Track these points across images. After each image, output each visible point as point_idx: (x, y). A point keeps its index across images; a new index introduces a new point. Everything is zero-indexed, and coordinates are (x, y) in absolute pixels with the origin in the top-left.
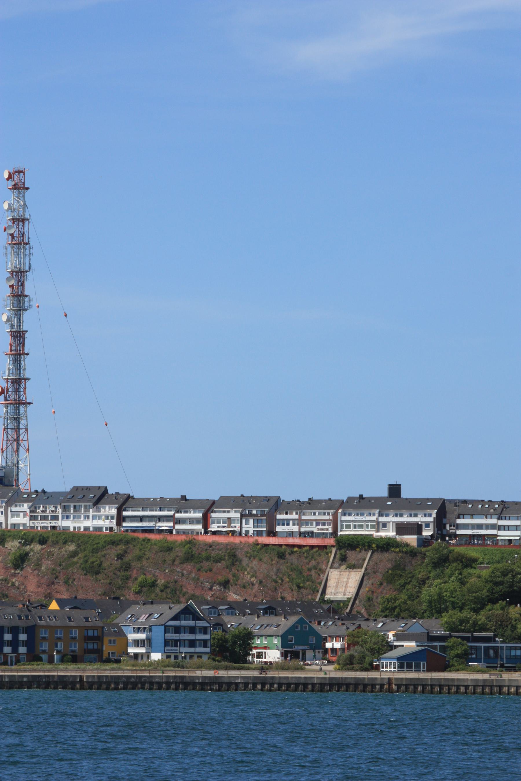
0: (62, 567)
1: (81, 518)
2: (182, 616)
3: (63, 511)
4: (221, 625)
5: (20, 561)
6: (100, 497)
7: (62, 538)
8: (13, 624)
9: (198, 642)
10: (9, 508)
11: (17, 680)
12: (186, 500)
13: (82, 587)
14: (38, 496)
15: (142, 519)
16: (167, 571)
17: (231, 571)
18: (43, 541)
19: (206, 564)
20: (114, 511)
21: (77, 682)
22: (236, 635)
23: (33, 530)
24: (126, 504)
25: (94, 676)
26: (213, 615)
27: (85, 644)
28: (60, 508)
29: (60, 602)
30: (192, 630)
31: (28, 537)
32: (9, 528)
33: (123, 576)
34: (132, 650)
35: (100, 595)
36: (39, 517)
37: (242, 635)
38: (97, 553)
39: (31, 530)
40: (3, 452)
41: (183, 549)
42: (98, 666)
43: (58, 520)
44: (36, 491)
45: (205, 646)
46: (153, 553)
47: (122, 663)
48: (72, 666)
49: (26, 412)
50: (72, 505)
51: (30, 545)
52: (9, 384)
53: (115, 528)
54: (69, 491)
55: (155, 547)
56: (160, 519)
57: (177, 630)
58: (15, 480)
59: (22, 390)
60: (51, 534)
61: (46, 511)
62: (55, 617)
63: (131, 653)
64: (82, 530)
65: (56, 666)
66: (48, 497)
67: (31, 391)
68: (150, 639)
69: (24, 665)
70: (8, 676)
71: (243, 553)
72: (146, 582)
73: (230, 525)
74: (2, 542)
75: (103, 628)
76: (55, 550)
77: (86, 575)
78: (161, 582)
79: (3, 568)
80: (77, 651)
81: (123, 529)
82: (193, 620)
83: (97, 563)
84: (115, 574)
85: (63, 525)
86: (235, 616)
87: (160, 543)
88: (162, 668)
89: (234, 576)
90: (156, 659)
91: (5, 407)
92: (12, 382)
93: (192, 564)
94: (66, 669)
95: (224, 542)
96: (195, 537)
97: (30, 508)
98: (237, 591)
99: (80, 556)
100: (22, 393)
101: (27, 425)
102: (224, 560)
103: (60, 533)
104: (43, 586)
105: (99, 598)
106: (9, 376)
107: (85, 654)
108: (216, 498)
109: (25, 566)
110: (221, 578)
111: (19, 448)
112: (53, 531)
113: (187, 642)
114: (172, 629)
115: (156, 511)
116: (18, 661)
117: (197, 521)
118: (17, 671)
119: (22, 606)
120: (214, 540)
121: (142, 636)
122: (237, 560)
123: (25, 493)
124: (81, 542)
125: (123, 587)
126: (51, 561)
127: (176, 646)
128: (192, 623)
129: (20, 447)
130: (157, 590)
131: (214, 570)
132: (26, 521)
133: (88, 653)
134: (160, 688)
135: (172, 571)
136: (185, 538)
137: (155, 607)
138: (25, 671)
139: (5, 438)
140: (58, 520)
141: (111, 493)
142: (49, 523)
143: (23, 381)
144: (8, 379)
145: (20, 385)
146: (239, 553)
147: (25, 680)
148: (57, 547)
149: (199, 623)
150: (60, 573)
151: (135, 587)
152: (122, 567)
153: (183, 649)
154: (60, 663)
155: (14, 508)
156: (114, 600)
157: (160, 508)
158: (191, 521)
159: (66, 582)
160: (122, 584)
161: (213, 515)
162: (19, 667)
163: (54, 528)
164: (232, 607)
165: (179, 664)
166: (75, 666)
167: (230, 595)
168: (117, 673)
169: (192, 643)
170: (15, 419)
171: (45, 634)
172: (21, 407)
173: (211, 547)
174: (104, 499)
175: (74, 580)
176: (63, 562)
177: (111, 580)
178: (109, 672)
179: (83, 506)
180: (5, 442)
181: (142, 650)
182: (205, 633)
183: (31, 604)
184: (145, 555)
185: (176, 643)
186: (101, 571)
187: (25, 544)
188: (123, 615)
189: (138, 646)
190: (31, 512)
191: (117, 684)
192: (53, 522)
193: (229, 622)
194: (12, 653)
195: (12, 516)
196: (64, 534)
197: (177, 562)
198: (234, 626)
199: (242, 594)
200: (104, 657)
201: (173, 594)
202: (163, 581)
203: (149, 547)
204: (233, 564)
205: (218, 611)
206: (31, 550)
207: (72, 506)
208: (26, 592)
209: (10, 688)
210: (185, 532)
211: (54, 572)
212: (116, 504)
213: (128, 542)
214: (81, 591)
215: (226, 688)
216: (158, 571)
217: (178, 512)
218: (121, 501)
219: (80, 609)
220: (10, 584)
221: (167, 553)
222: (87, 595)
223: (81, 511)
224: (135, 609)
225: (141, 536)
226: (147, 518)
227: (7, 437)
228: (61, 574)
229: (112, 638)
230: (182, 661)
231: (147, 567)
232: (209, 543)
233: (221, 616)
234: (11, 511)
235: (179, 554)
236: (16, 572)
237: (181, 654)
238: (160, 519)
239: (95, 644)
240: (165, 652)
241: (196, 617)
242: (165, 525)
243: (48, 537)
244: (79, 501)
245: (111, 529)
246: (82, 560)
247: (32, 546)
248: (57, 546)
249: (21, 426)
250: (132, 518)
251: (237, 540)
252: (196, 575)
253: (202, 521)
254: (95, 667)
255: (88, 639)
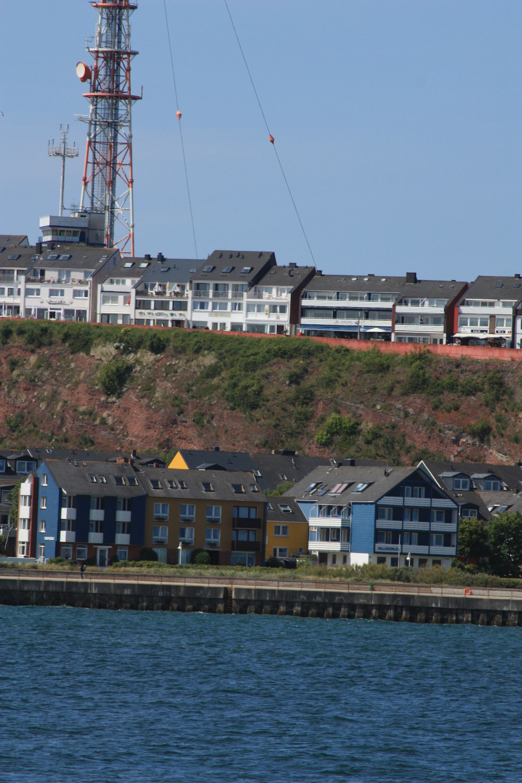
0: (190, 394)
1: (226, 309)
2: (408, 489)
3: (196, 295)
4: (477, 507)
5: (117, 380)
6: (262, 270)
7: (193, 342)
8: (108, 493)
9: (434, 536)
10: (99, 286)
11: (113, 592)
12: (416, 281)
13: (226, 431)
14: (151, 266)
15: (335, 312)
16: (378, 407)
17: (493, 410)
18: (158, 346)
19: (448, 397)
20: (286, 298)
21: (218, 600)
22: (502, 524)
23: (140, 327)
24: (308, 286)
25: (249, 590)
26: (461, 489)
27: (234, 532)
28: (191, 289)
29: (188, 456)
30: (425, 514)
31: (132, 339)
32: (98, 321)
33: (300, 413)
34: (316, 546)
35: (257, 446)
36: (153, 303)
37: (513, 525)
38: (254, 371)
39: (137, 326)
40: (86, 184)
41: (408, 370)
42: (257, 573)
43: (186, 310)
44: (148, 257)
45: (447, 544)
46: (353, 374)
47: (299, 569)
48: (211, 571)
49: (128, 113)
50: (212, 283)
51: (135, 353)
52: (101, 60)
53: (287, 327)
54: (206, 258)
55: (357, 363)
56: (368, 313)
57: (398, 513)
58: (107, 235)
59: (122, 73)
60: (173, 334)
61: (165, 293)
62: (181, 483)
63: (315, 551)
64: (228, 328)
65: (181, 570)
66: (169, 269)
67: (139, 76)
68: (348, 529)
69: (125, 565)
70: (97, 584)
71: (517, 380)
72: (340, 425)
73: (495, 327)
74: (84, 345)
75: (266, 504)
76: (179, 362)
77: (233, 409)
78: (367, 426)
79: (86, 391)
80: (219, 545)
81: (301, 330)
82: (426, 497)
83: (254, 388)
84: (284, 410)
85: (194, 319)
86: (501, 493)
87: (368, 358)
88: (371, 581)
89: (499, 420)
90: (361, 564)
91: (92, 102)
92: (105, 58)
93: (423, 395)
94: (201, 577)
95: (483, 358)
96: (431, 348)
97: (136, 287)
98: (503, 447)
99: (223, 374)
100: (122, 79)
101: (131, 137)
102: (481, 390)
103: (189, 334)
104: (157, 426)
105: (256, 450)
106: (100, 46)
107: (233, 549)
108: (470, 278)
109: (125, 389)
110: (475, 423)
111: (114, 178)
112: (177, 330)
113: (415, 536)
114: (389, 511)
115: (362, 299)
116: (114, 559)
117: (435, 320)
118: (113, 576)
119: (122, 461)
120: (464, 353)
121: (335, 522)
122: (504, 392)
123: (127, 260)
124: (227, 352)
125: (299, 433)
126: (172, 382)
127: (395, 542)
128: (423, 502)
129: (117, 176)
130: (360, 440)
131: (463, 408)
132: (130, 310)
133: (238, 549)
134: (367, 615)
135: (387, 408)
136: (413, 350)
137: (358, 471)
138: (127, 576)
139: (91, 160)
140: (186, 310)
141: (282, 265)
142: (169, 315)
143: (125, 56)
144: (97, 52)
145: (119, 64)
146: (509, 380)
147: (127, 592)
148: (184, 358)
149: (438, 503)
150: (187, 404)
151: (320, 434)
152: (297, 398)
153: (408, 548)
154: (189, 565)
155: (107, 287)
156: (286, 457)
157: (369, 294)
158: (424, 319)
159: (198, 422)
160: (298, 427)
161: (464, 309)
162: (117, 569)
163: (178, 323)
164: (496, 476)
165: (401, 573)
166: (215, 571)
167: (491, 453)
168: (291, 586)
169: (424, 538)
170: (109, 125)
171: (163, 512)
172: (120, 104)
173: (458, 366)
174: (268, 275)
175: (212, 418)
176: (193, 385)
177: (278, 419)
178: (276, 583)
179: (230, 287)
180: (90, 166)
181: (335, 547)
182: (449, 520)
183: (138, 458)
184: (339, 377)
185: (395, 536)
186: (261, 403)
187: (126, 351)
188: (301, 483)
189: (327, 540)
190: (138, 293)
191: (290, 605)
192: (177, 313)
193: (489, 502)
194: (104, 544)
195: (105, 300)
196: (196, 336)
197: (397, 392)
198: (498, 510)
199: (513, 453)
200: (267, 557)
201: (388, 448)
202: (370, 425)
203: (347, 363)
204: (498, 399)
205: (471, 481)
206: (137, 361)
207: (211, 286)
208: (127, 436)
209: (100, 607)
210: (412, 339)
211: (177, 402)
212: (290, 285)
213: (309, 354)
214: (224, 439)
215: (408, 616)
216: (362, 406)
217: (401, 302)
218: (300, 279)
219: (225, 469)
220: (98, 422)
221: (380, 374)
222: (234, 445)
223: (227, 295)
224: (323, 473)
225: (334, 343)
226: (345, 312)
227: (95, 158)
228: (190, 407)
229: (282, 524)
230: (407, 569)
231: (342, 399)
232: (456, 360)
233: (476, 491)
234: (102, 291)
235: (401, 378)
236: (110, 400)
237: (403, 556)
238: (368, 313)
239: (250, 532)
240: (375, 552)
241: (432, 492)
242: (377, 325)
243: (168, 340)
244: (224, 277)
245: (281, 328)
246: (227, 382)
247: (139, 355)
248: (182, 356)
249: (120, 139)
250: (318, 312)
251: (506, 355)
252: (430, 416)
253: (443, 320)
254: (252, 573)
255: (240, 523)
